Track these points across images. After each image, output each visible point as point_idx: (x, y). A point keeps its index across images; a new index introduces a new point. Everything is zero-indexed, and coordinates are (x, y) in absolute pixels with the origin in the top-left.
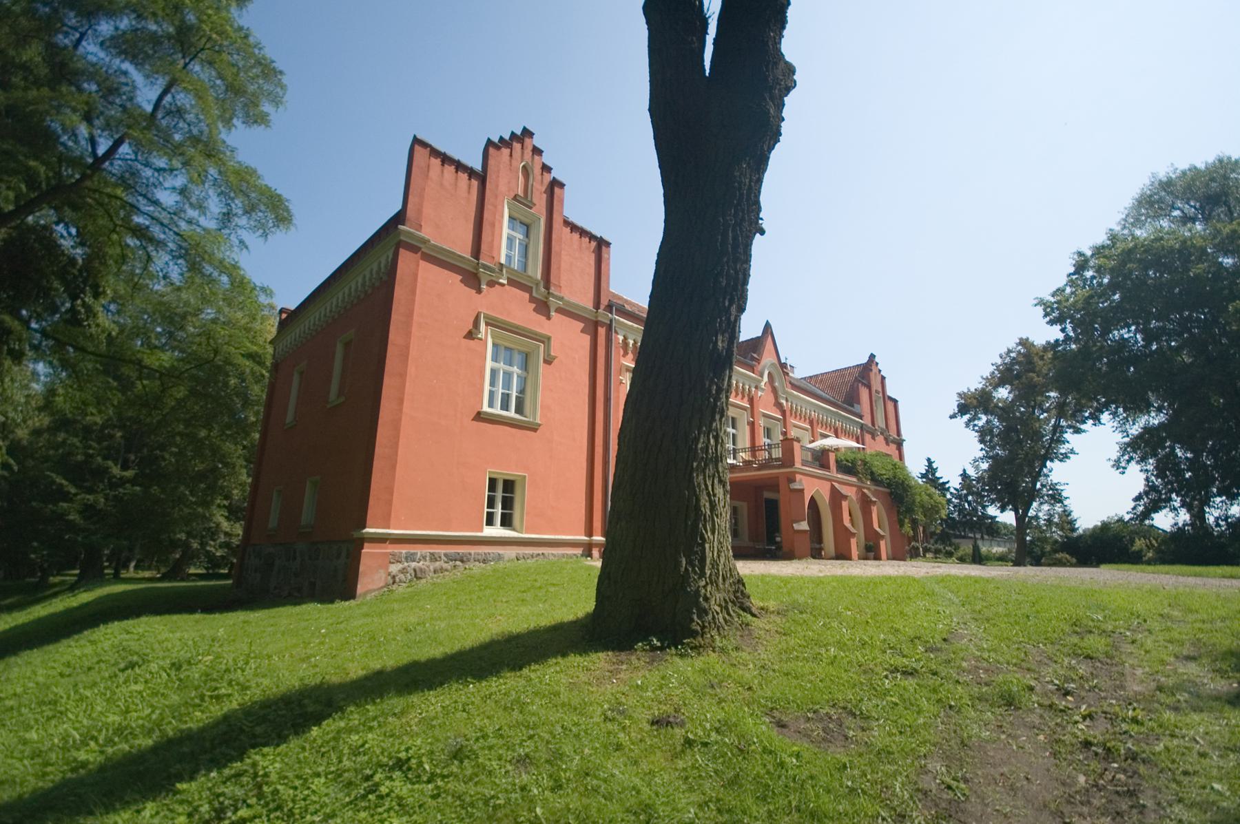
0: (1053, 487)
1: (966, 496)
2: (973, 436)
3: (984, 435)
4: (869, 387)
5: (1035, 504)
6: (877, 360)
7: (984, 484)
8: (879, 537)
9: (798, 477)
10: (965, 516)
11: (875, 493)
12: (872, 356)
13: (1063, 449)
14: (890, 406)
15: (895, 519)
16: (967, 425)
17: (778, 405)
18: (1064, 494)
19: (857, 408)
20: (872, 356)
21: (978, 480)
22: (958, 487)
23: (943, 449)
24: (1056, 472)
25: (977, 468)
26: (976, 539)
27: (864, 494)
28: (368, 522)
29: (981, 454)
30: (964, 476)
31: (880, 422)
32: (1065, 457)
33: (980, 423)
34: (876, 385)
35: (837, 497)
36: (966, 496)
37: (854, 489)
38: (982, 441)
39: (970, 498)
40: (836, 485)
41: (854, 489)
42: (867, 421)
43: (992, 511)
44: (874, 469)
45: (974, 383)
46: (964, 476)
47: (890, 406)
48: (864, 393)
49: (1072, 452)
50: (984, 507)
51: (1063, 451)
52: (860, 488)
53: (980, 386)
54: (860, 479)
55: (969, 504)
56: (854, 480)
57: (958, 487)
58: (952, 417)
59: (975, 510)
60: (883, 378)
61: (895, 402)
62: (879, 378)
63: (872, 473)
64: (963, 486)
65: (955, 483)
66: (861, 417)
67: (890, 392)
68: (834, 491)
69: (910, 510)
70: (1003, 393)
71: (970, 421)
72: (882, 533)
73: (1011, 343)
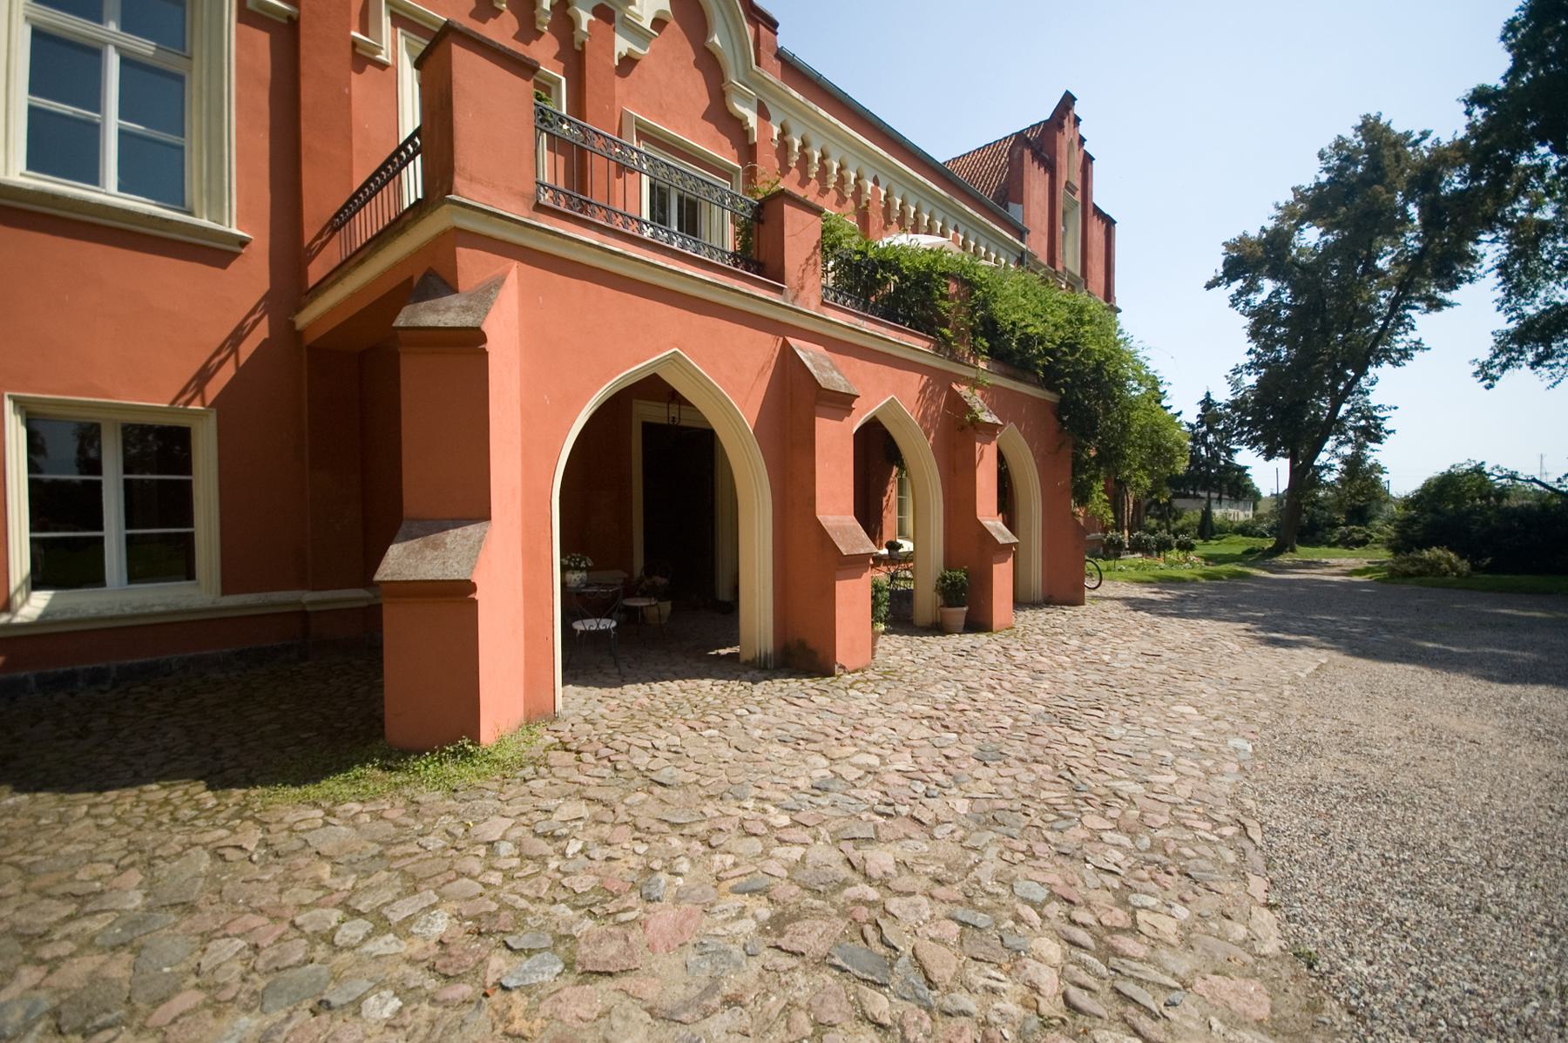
0: (1368, 414)
1: (1205, 435)
2: (1241, 323)
3: (1262, 323)
4: (1051, 167)
5: (1328, 445)
6: (1078, 109)
7: (1245, 413)
8: (989, 549)
9: (471, 265)
10: (1198, 468)
11: (999, 401)
12: (1068, 100)
13: (1401, 341)
14: (1097, 230)
15: (1064, 480)
16: (1234, 303)
17: (722, 118)
18: (1387, 425)
19: (1014, 211)
20: (1068, 100)
21: (1235, 405)
22: (1194, 421)
23: (1188, 346)
24: (1385, 385)
25: (1236, 385)
26: (1210, 499)
27: (956, 402)
28: (414, 497)
29: (1247, 360)
30: (1207, 403)
31: (1070, 260)
32: (1405, 354)
33: (1258, 299)
34: (1068, 171)
35: (795, 400)
36: (1205, 435)
37: (916, 381)
38: (1254, 334)
39: (1211, 438)
40: (807, 352)
41: (916, 381)
42: (1037, 244)
43: (1246, 457)
44: (999, 308)
45: (1256, 221)
46: (1207, 403)
47: (1097, 230)
48: (1036, 182)
49: (1418, 345)
50: (1230, 452)
51: (1401, 346)
52: (940, 381)
53: (1270, 225)
54: (943, 345)
55: (1208, 447)
56: (921, 344)
57: (1194, 421)
58: (1209, 286)
59: (1216, 456)
60: (1088, 159)
61: (1109, 223)
62: (1078, 159)
63: (990, 328)
64: (1203, 419)
65: (1502, 85)
66: (1021, 233)
67: (1101, 198)
68: (789, 371)
69: (1110, 457)
70: (1311, 236)
71: (1240, 293)
72: (1002, 534)
73: (1346, 128)
